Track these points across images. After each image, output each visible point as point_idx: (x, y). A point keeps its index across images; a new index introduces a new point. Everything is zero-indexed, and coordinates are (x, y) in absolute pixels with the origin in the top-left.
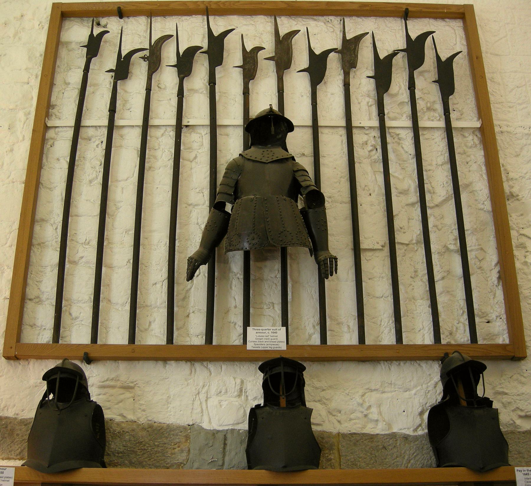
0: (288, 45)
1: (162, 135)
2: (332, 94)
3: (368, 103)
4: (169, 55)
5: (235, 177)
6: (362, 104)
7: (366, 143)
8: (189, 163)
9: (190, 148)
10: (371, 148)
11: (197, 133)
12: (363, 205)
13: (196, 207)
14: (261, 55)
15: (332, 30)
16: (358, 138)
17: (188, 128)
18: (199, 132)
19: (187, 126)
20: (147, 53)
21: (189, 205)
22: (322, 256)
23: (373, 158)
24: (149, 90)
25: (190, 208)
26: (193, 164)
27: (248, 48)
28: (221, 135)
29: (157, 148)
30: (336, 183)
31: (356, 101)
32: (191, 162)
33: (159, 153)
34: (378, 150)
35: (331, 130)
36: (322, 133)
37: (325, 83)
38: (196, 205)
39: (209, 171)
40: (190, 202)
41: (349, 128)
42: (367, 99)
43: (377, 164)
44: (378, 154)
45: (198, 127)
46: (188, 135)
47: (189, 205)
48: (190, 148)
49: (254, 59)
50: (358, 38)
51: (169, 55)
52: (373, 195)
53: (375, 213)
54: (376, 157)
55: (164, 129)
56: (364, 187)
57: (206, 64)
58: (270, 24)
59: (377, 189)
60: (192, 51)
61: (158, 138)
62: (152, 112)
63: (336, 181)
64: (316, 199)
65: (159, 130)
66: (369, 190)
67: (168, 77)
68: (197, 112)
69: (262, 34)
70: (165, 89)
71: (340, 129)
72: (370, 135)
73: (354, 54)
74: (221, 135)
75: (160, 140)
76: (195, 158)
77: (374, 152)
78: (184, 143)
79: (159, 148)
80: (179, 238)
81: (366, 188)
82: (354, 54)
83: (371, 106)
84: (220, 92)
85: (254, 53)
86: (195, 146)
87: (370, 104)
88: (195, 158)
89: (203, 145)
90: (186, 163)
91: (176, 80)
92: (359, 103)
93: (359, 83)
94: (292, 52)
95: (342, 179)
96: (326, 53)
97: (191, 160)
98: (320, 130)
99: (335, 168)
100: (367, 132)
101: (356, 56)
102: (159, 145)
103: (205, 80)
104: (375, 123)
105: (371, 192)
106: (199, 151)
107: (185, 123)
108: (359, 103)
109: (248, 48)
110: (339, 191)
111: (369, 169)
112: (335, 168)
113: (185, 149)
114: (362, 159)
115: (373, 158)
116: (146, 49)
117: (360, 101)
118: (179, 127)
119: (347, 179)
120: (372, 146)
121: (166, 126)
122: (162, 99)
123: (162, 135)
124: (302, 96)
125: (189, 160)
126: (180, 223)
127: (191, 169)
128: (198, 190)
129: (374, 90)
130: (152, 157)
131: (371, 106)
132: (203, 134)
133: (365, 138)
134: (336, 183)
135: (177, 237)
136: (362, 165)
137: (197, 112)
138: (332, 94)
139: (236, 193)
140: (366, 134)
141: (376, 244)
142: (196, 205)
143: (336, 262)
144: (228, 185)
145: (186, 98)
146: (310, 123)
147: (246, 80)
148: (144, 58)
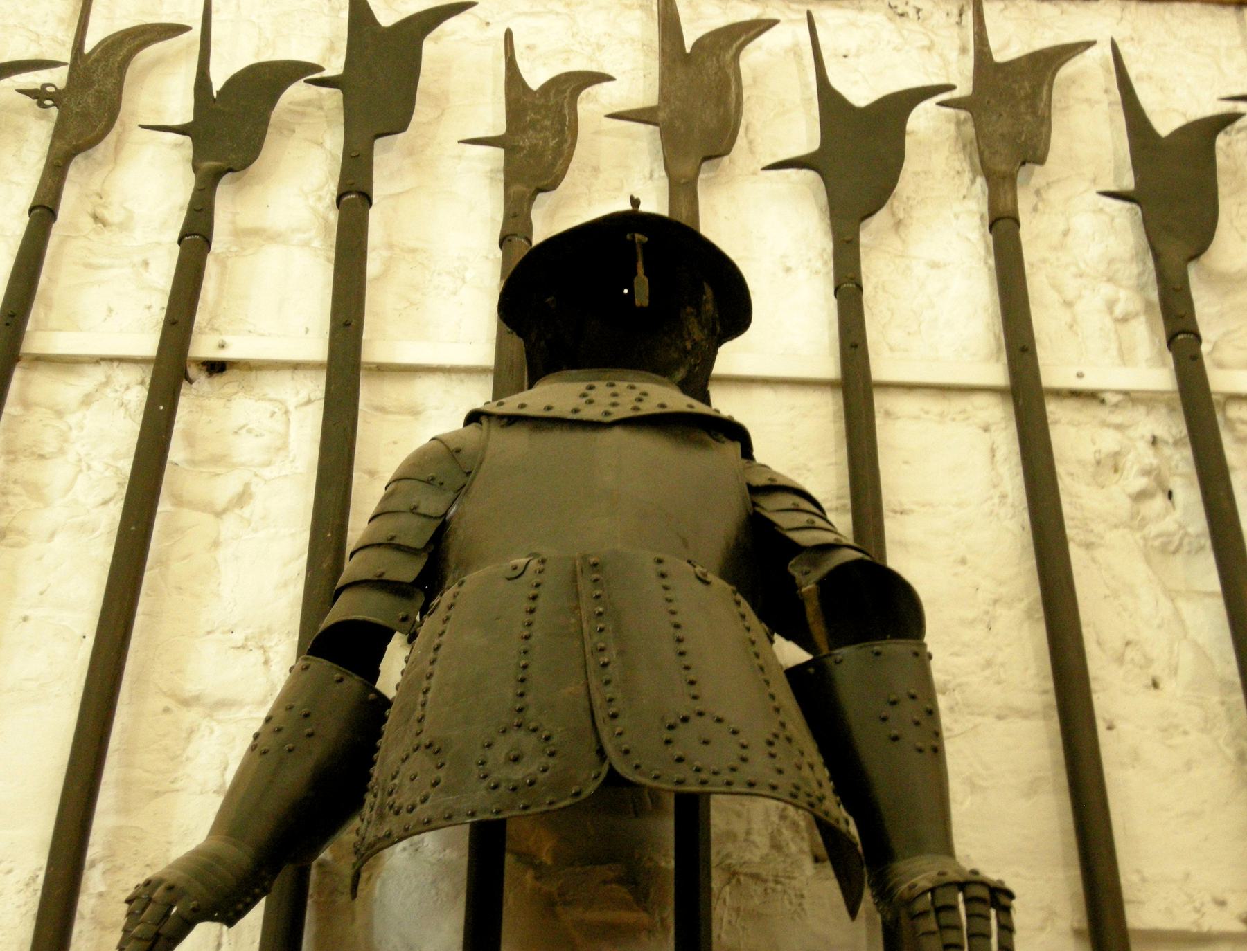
0: (721, 68)
1: (87, 401)
2: (935, 265)
3: (1111, 305)
4: (163, 92)
5: (433, 504)
6: (1079, 307)
7: (1114, 463)
8: (206, 518)
9: (216, 460)
10: (1142, 483)
11: (263, 398)
12: (1120, 726)
13: (221, 714)
14: (592, 106)
15: (926, 42)
16: (1072, 437)
17: (218, 380)
18: (272, 395)
19: (216, 367)
20: (58, 78)
21: (186, 703)
22: (917, 873)
23: (1153, 529)
24: (44, 212)
25: (191, 716)
26: (230, 524)
27: (535, 77)
28: (381, 409)
29: (47, 450)
30: (972, 623)
31: (1052, 297)
32: (219, 514)
33: (55, 474)
34: (1179, 496)
35: (934, 405)
36: (888, 414)
37: (898, 224)
38: (222, 704)
39: (305, 557)
40: (191, 689)
41: (1026, 396)
42: (1107, 290)
43: (1178, 560)
44: (1178, 514)
45: (268, 377)
46: (214, 403)
47: (186, 703)
48: (216, 460)
49: (560, 113)
50: (1047, 62)
51: (163, 92)
52: (1167, 685)
53: (1189, 765)
54: (1169, 524)
55: (97, 375)
56: (1118, 644)
57: (334, 140)
58: (638, 13)
59: (1187, 658)
60: (266, 82)
61: (60, 414)
62: (49, 307)
63: (970, 614)
64: (876, 604)
65: (72, 379)
66: (1149, 661)
67: (146, 178)
68: (272, 299)
69: (600, 47)
70: (124, 226)
71: (981, 400)
72: (1131, 433)
73: (1035, 113)
74: (381, 409)
75: (72, 419)
76: (243, 498)
77: (1159, 501)
78: (190, 440)
79: (61, 451)
80: (110, 855)
81: (1130, 653)
82: (1035, 113)
83: (1124, 319)
84: (391, 247)
85: (560, 92)
86: (246, 449)
87: (1119, 310)
88: (243, 498)
89: (284, 447)
90: (189, 516)
91: (182, 186)
92: (1068, 304)
93: (1062, 227)
94: (739, 95)
95: (1000, 611)
96: (898, 106)
97: (219, 507)
98: (881, 402)
99: (963, 562)
100: (1117, 418)
101: (1044, 122)
102: (64, 438)
103: (320, 198)
104: (1159, 376)
105: (1157, 670)
106: (267, 472)
107: (203, 347)
108: (1068, 304)
109: (535, 77)
110: (989, 664)
111: (1137, 571)
112: (963, 562)
113: (193, 462)
114: (1099, 528)
115: (1153, 529)
116: (65, 64)
117: (1070, 295)
118: (176, 367)
119: (1029, 614)
120: (1146, 472)
121: (111, 360)
122: (105, 261)
123: (87, 401)
124: (788, 270)
125: (207, 507)
126: (126, 784)
127: (216, 544)
128: (238, 637)
129: (1136, 257)
130: (18, 489)
131: (1124, 319)
132: (292, 402)
133: (1109, 441)
134: (972, 623)
135: (92, 852)
136: (1099, 554)
137: (272, 299)
138: (935, 265)
139: (430, 566)
140: (1119, 427)
141: (1210, 908)
142: (222, 704)
143: (1005, 910)
144: (392, 545)
145: (223, 264)
146: (828, 366)
147: (517, 188)
148: (39, 95)
